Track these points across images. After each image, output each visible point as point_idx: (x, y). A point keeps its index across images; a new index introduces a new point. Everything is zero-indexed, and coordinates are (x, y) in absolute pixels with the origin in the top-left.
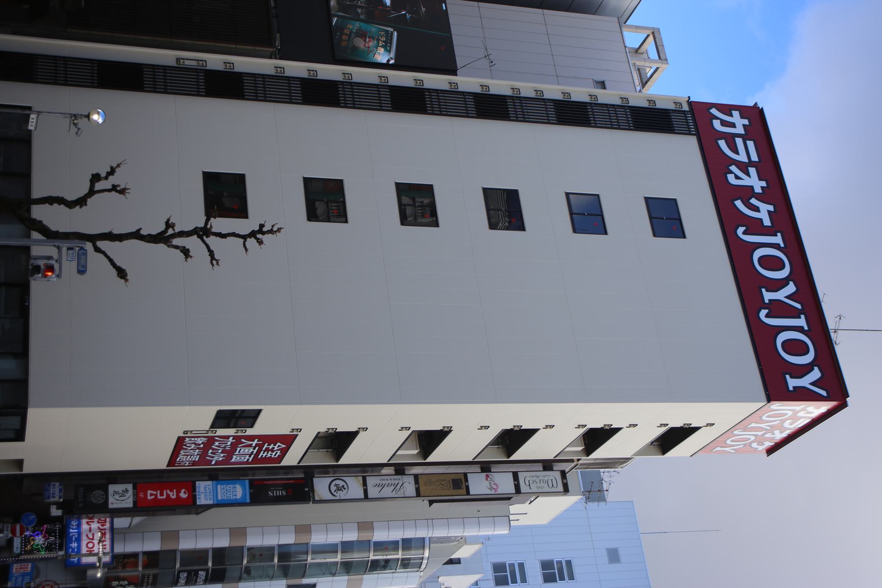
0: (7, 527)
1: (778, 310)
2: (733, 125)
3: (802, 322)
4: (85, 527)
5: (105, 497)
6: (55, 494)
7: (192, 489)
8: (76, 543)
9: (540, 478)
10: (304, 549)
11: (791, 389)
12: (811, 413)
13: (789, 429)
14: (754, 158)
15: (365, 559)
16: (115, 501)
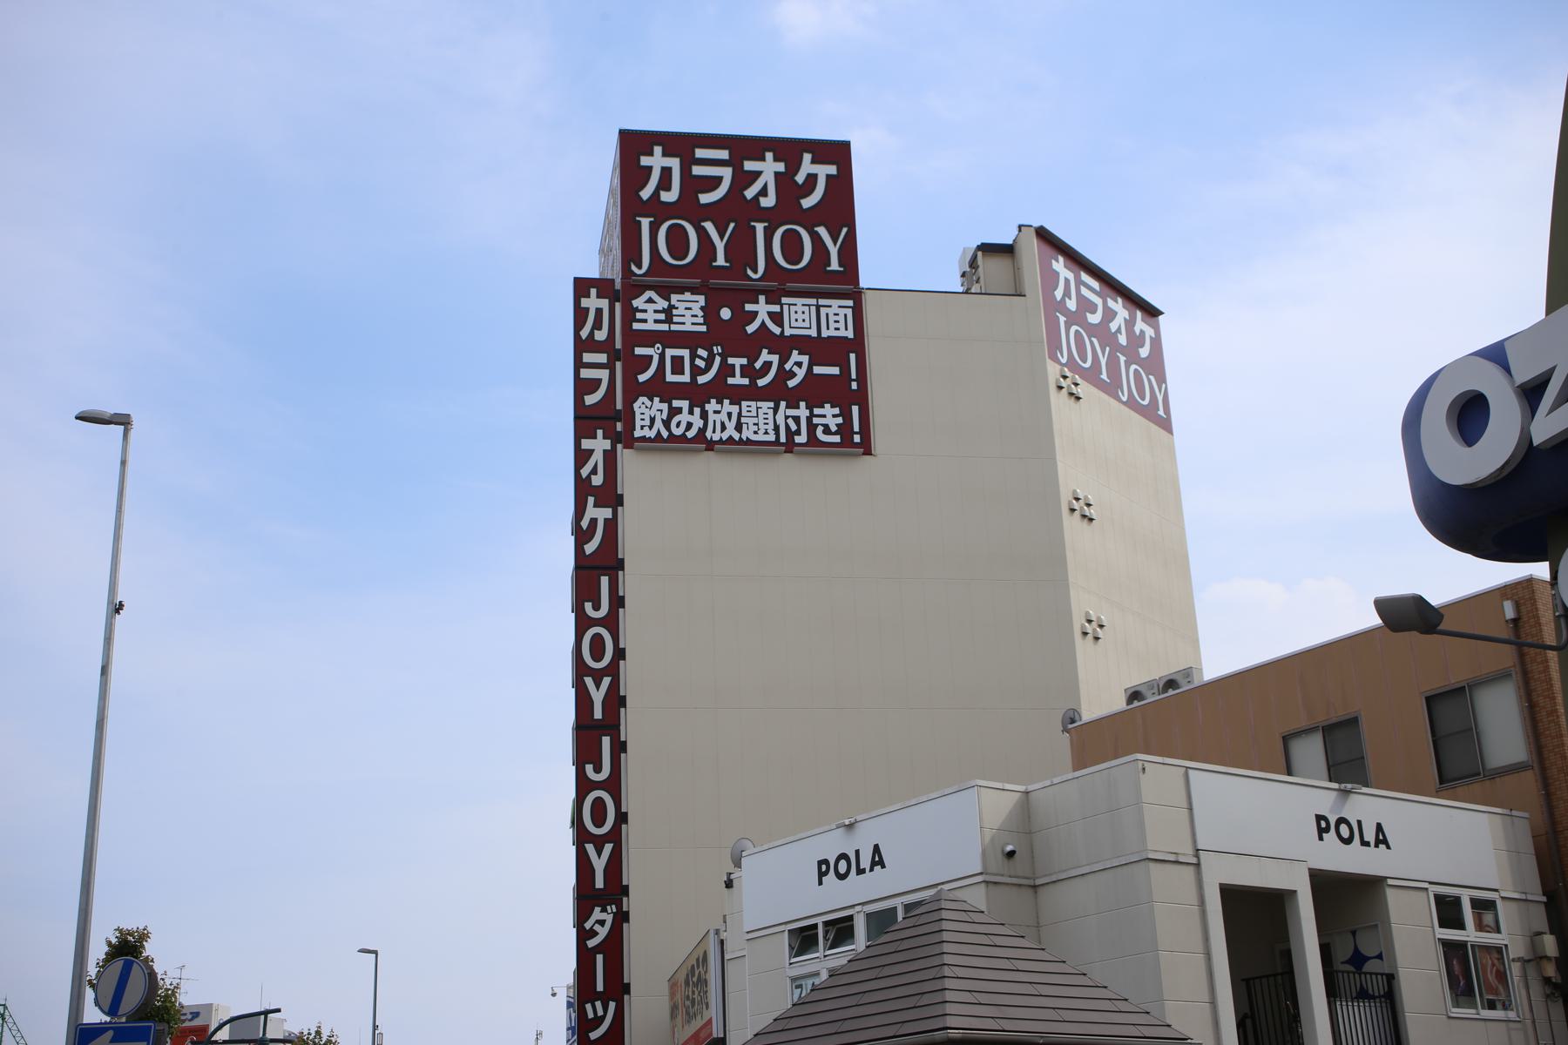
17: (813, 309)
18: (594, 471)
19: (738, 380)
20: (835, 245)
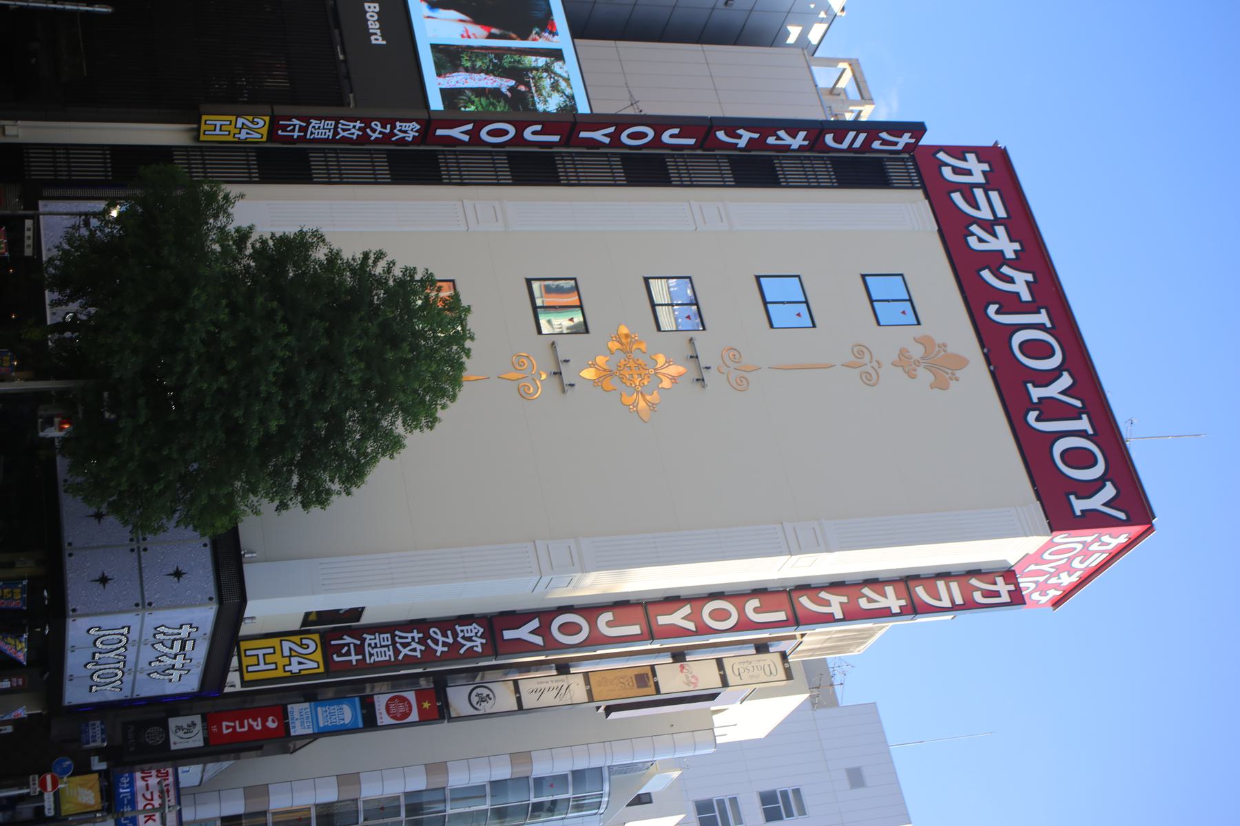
0: (34, 780)
1: (1050, 410)
3: (1084, 424)
4: (140, 784)
5: (164, 735)
6: (95, 736)
7: (283, 715)
8: (129, 806)
9: (752, 664)
10: (439, 796)
11: (1078, 513)
12: (1108, 544)
13: (1079, 570)
14: (1001, 213)
15: (523, 803)
16: (178, 740)
18: (870, 600)
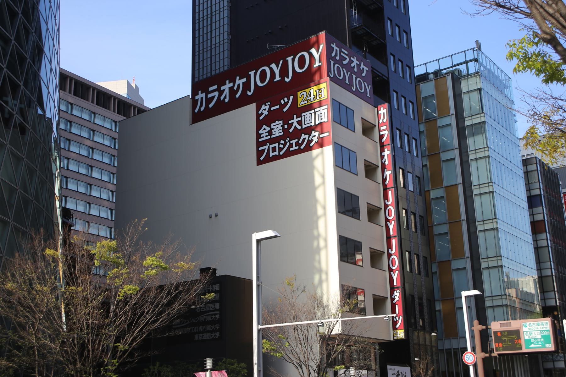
2: (202, 98)
14: (215, 87)
17: (313, 114)
19: (295, 148)
20: (278, 68)
